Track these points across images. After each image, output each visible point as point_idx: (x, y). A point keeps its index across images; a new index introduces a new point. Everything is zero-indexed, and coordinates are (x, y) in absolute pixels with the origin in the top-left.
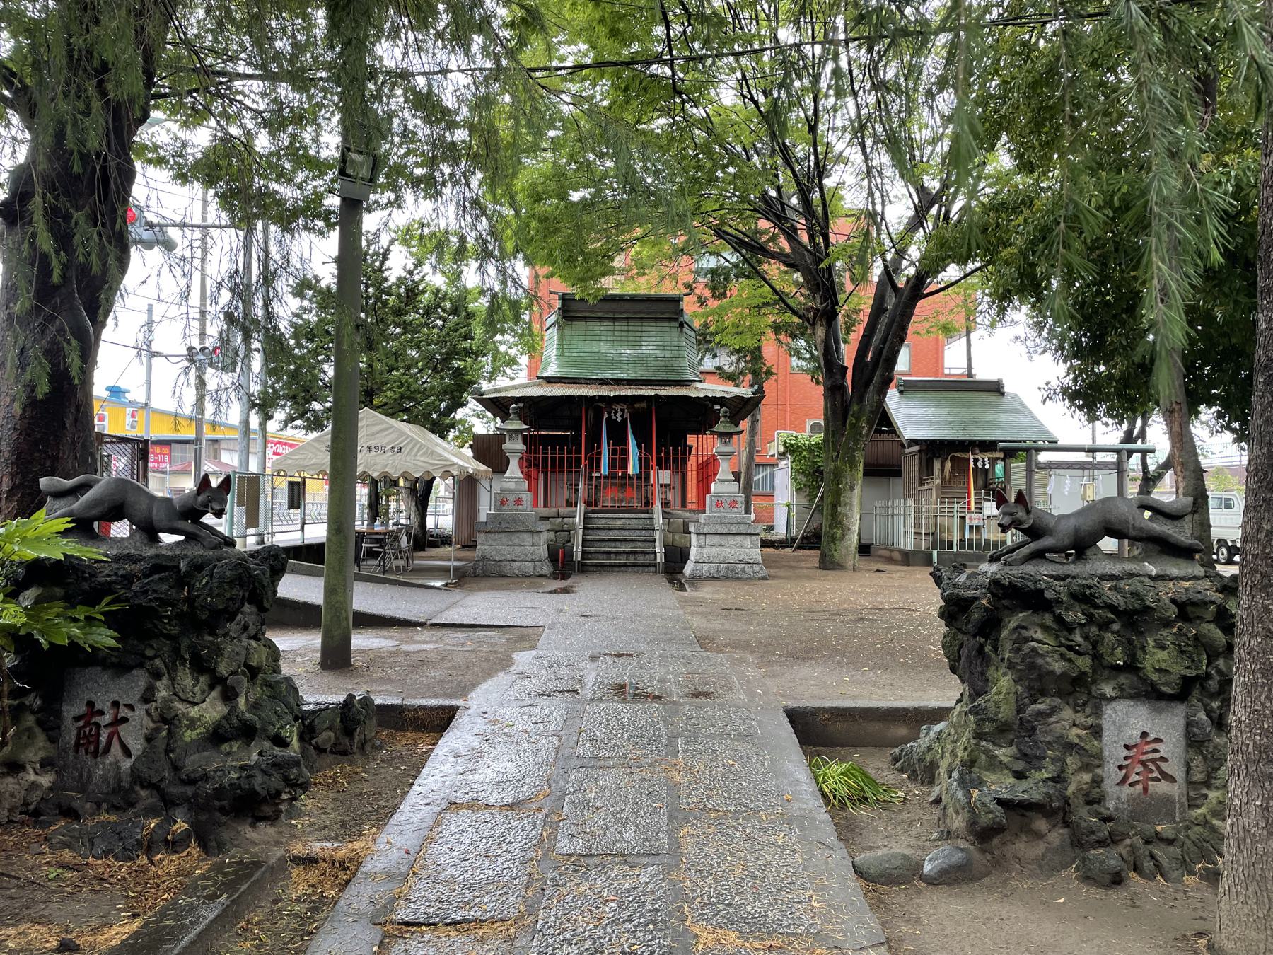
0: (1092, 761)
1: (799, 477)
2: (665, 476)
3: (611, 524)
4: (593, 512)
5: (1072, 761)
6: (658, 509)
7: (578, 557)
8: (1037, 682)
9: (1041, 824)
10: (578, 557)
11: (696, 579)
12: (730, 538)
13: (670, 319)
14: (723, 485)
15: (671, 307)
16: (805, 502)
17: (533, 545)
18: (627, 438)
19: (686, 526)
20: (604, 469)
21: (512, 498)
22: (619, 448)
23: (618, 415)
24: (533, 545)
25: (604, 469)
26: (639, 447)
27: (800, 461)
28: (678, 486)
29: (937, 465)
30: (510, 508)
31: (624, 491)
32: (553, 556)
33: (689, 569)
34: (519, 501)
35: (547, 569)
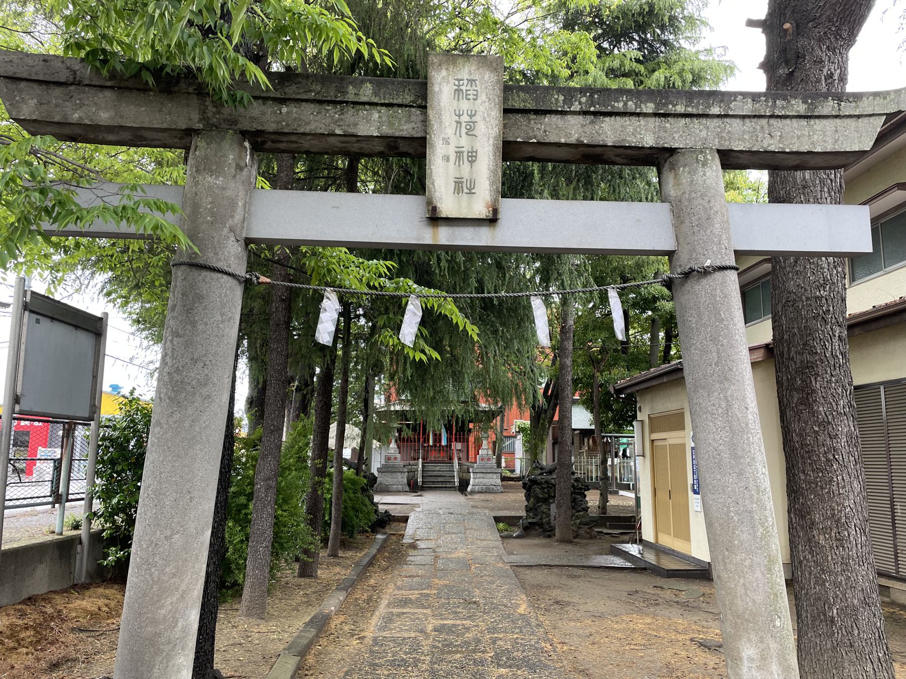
0: (549, 516)
2: (459, 446)
3: (434, 469)
5: (544, 516)
6: (456, 461)
7: (420, 484)
8: (538, 500)
9: (537, 527)
10: (420, 484)
11: (472, 492)
14: (485, 450)
19: (468, 469)
25: (431, 443)
28: (465, 450)
29: (586, 440)
30: (391, 463)
32: (409, 484)
33: (469, 489)
34: (396, 458)
35: (407, 489)
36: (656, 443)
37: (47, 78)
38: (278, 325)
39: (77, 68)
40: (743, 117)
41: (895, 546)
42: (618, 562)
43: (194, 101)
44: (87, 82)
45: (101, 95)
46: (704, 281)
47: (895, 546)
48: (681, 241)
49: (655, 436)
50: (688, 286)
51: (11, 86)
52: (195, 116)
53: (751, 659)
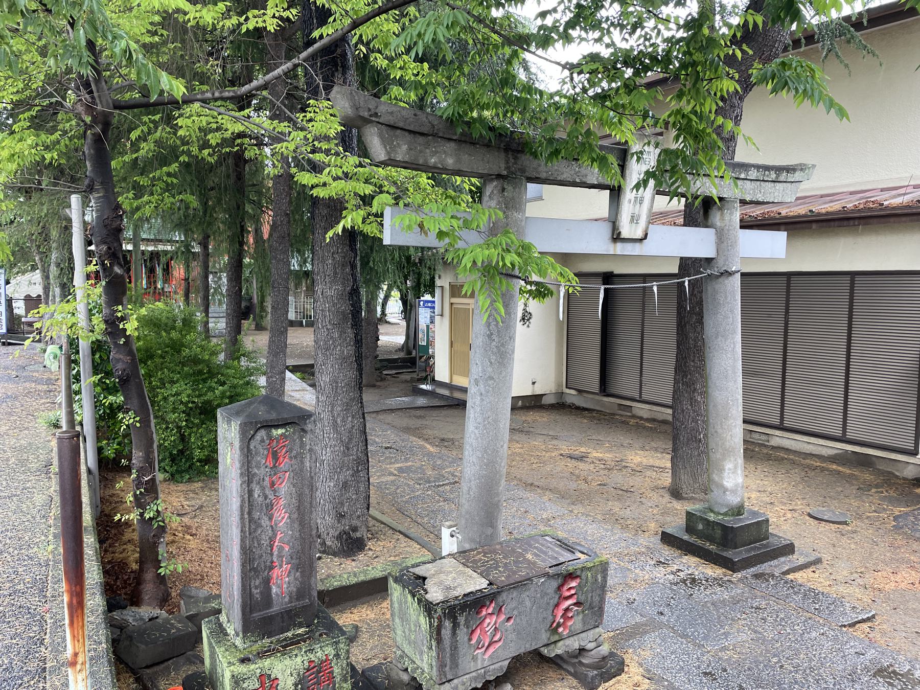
36: (454, 306)
37: (417, 129)
38: (283, 237)
39: (436, 123)
40: (751, 180)
41: (641, 381)
42: (421, 401)
43: (503, 155)
44: (441, 135)
45: (448, 145)
46: (730, 278)
47: (641, 381)
48: (720, 253)
49: (454, 300)
50: (720, 280)
51: (391, 133)
52: (503, 166)
53: (729, 469)
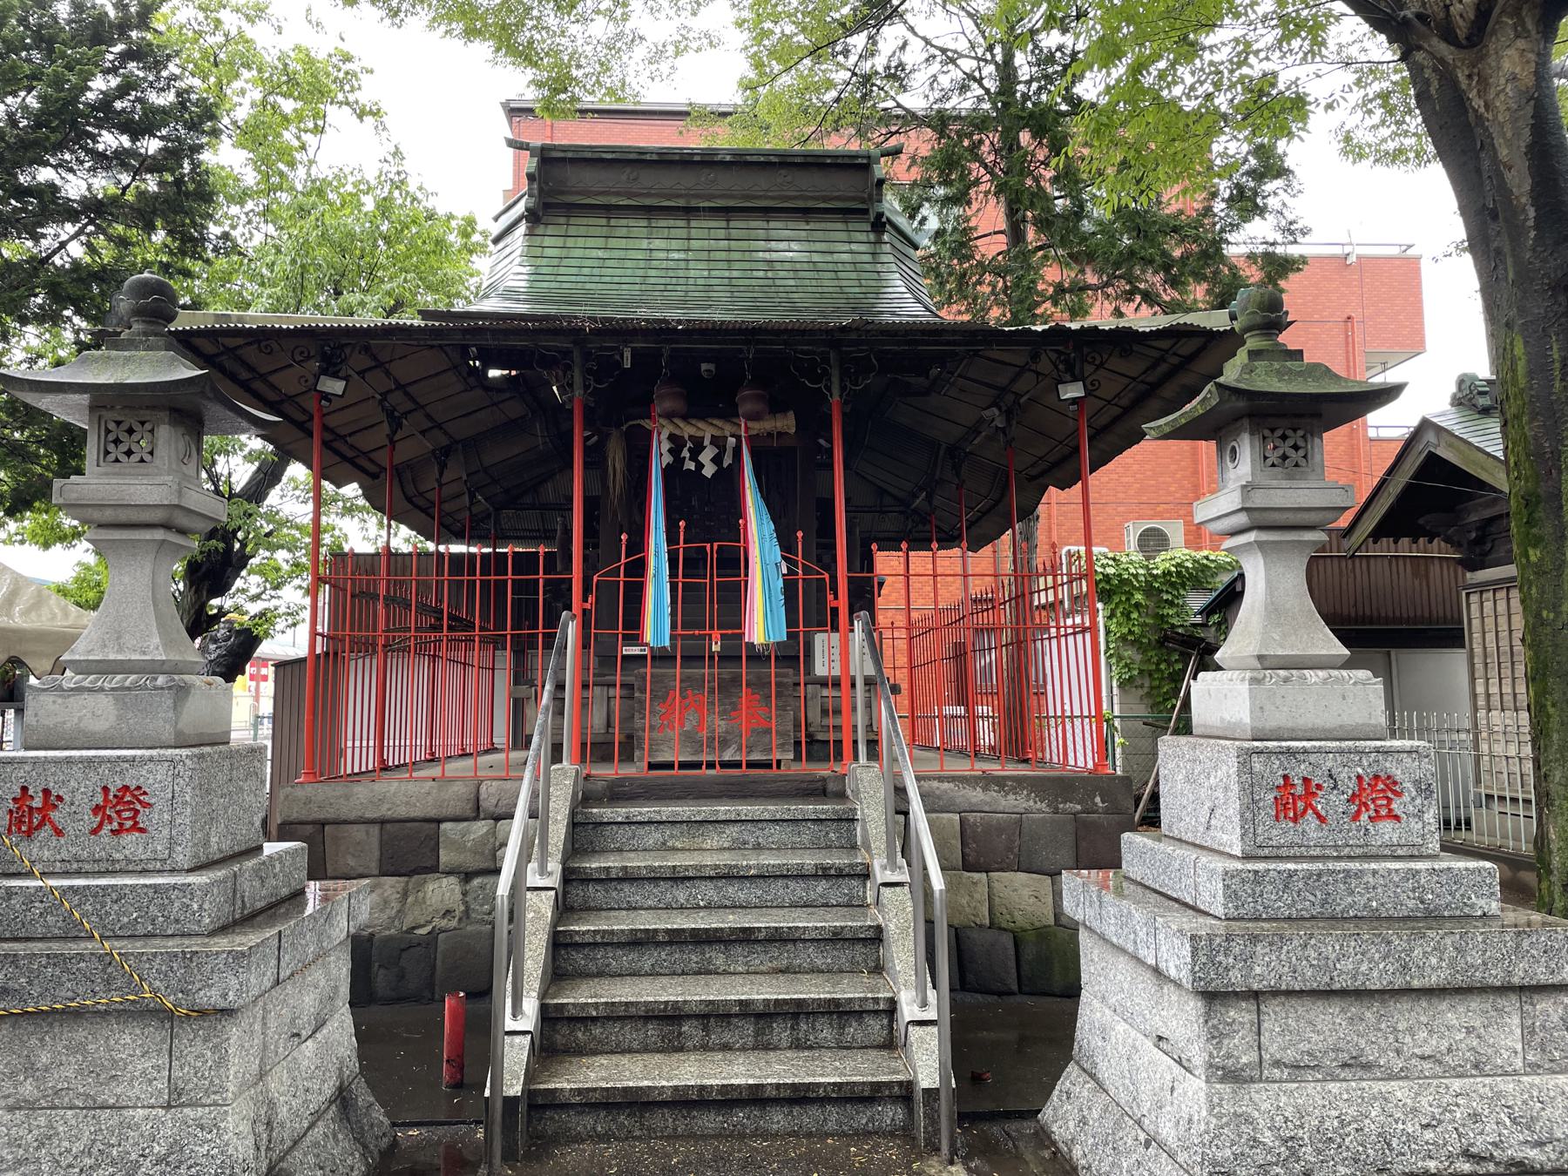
1: (1129, 653)
4: (617, 793)
12: (1405, 1015)
13: (846, 214)
15: (843, 185)
16: (1142, 710)
17: (175, 1099)
18: (738, 511)
20: (657, 626)
21: (80, 794)
22: (712, 548)
23: (706, 457)
24: (175, 1099)
26: (787, 545)
27: (1127, 615)
31: (731, 711)
